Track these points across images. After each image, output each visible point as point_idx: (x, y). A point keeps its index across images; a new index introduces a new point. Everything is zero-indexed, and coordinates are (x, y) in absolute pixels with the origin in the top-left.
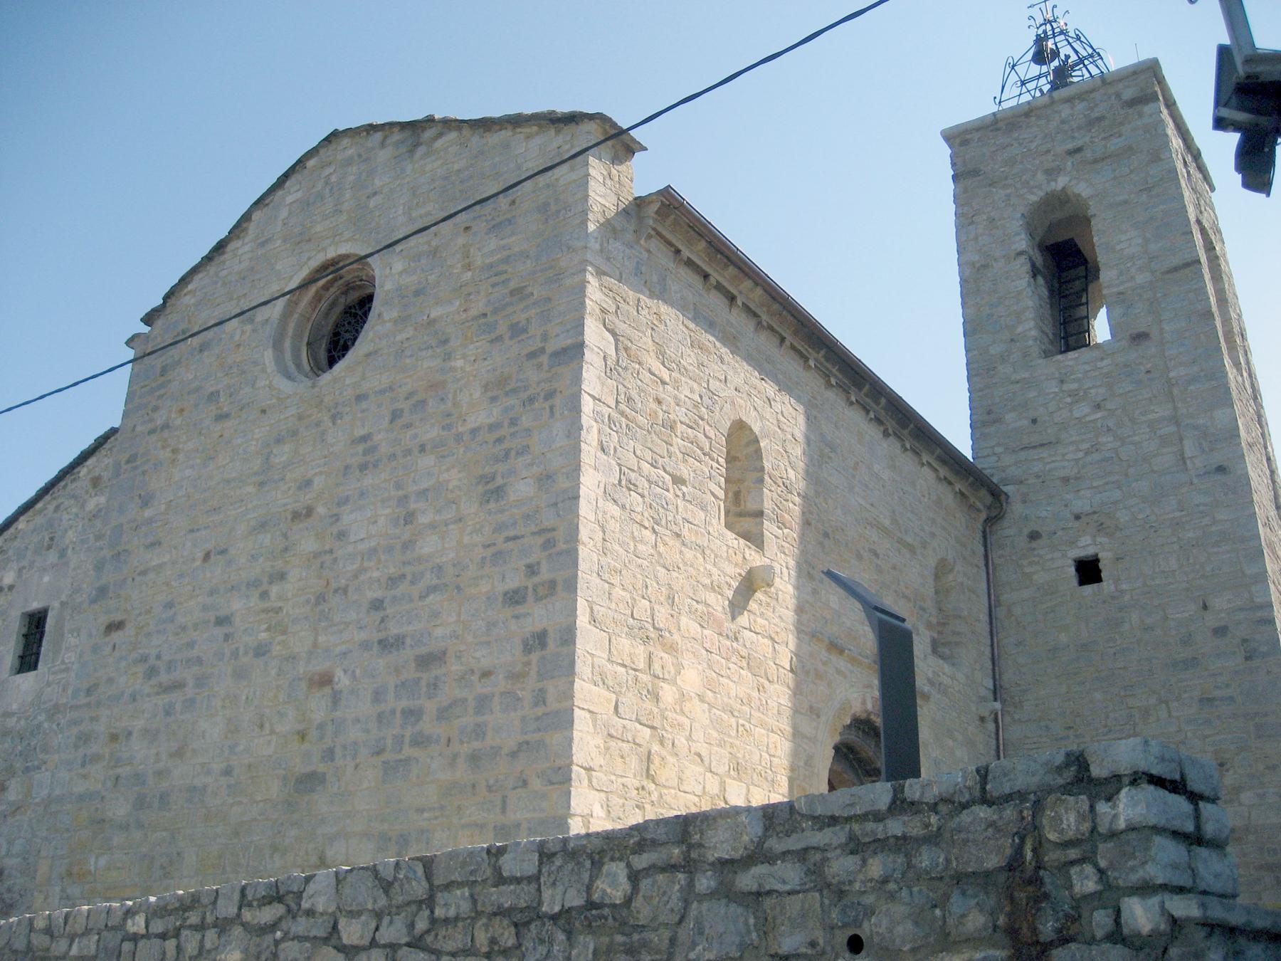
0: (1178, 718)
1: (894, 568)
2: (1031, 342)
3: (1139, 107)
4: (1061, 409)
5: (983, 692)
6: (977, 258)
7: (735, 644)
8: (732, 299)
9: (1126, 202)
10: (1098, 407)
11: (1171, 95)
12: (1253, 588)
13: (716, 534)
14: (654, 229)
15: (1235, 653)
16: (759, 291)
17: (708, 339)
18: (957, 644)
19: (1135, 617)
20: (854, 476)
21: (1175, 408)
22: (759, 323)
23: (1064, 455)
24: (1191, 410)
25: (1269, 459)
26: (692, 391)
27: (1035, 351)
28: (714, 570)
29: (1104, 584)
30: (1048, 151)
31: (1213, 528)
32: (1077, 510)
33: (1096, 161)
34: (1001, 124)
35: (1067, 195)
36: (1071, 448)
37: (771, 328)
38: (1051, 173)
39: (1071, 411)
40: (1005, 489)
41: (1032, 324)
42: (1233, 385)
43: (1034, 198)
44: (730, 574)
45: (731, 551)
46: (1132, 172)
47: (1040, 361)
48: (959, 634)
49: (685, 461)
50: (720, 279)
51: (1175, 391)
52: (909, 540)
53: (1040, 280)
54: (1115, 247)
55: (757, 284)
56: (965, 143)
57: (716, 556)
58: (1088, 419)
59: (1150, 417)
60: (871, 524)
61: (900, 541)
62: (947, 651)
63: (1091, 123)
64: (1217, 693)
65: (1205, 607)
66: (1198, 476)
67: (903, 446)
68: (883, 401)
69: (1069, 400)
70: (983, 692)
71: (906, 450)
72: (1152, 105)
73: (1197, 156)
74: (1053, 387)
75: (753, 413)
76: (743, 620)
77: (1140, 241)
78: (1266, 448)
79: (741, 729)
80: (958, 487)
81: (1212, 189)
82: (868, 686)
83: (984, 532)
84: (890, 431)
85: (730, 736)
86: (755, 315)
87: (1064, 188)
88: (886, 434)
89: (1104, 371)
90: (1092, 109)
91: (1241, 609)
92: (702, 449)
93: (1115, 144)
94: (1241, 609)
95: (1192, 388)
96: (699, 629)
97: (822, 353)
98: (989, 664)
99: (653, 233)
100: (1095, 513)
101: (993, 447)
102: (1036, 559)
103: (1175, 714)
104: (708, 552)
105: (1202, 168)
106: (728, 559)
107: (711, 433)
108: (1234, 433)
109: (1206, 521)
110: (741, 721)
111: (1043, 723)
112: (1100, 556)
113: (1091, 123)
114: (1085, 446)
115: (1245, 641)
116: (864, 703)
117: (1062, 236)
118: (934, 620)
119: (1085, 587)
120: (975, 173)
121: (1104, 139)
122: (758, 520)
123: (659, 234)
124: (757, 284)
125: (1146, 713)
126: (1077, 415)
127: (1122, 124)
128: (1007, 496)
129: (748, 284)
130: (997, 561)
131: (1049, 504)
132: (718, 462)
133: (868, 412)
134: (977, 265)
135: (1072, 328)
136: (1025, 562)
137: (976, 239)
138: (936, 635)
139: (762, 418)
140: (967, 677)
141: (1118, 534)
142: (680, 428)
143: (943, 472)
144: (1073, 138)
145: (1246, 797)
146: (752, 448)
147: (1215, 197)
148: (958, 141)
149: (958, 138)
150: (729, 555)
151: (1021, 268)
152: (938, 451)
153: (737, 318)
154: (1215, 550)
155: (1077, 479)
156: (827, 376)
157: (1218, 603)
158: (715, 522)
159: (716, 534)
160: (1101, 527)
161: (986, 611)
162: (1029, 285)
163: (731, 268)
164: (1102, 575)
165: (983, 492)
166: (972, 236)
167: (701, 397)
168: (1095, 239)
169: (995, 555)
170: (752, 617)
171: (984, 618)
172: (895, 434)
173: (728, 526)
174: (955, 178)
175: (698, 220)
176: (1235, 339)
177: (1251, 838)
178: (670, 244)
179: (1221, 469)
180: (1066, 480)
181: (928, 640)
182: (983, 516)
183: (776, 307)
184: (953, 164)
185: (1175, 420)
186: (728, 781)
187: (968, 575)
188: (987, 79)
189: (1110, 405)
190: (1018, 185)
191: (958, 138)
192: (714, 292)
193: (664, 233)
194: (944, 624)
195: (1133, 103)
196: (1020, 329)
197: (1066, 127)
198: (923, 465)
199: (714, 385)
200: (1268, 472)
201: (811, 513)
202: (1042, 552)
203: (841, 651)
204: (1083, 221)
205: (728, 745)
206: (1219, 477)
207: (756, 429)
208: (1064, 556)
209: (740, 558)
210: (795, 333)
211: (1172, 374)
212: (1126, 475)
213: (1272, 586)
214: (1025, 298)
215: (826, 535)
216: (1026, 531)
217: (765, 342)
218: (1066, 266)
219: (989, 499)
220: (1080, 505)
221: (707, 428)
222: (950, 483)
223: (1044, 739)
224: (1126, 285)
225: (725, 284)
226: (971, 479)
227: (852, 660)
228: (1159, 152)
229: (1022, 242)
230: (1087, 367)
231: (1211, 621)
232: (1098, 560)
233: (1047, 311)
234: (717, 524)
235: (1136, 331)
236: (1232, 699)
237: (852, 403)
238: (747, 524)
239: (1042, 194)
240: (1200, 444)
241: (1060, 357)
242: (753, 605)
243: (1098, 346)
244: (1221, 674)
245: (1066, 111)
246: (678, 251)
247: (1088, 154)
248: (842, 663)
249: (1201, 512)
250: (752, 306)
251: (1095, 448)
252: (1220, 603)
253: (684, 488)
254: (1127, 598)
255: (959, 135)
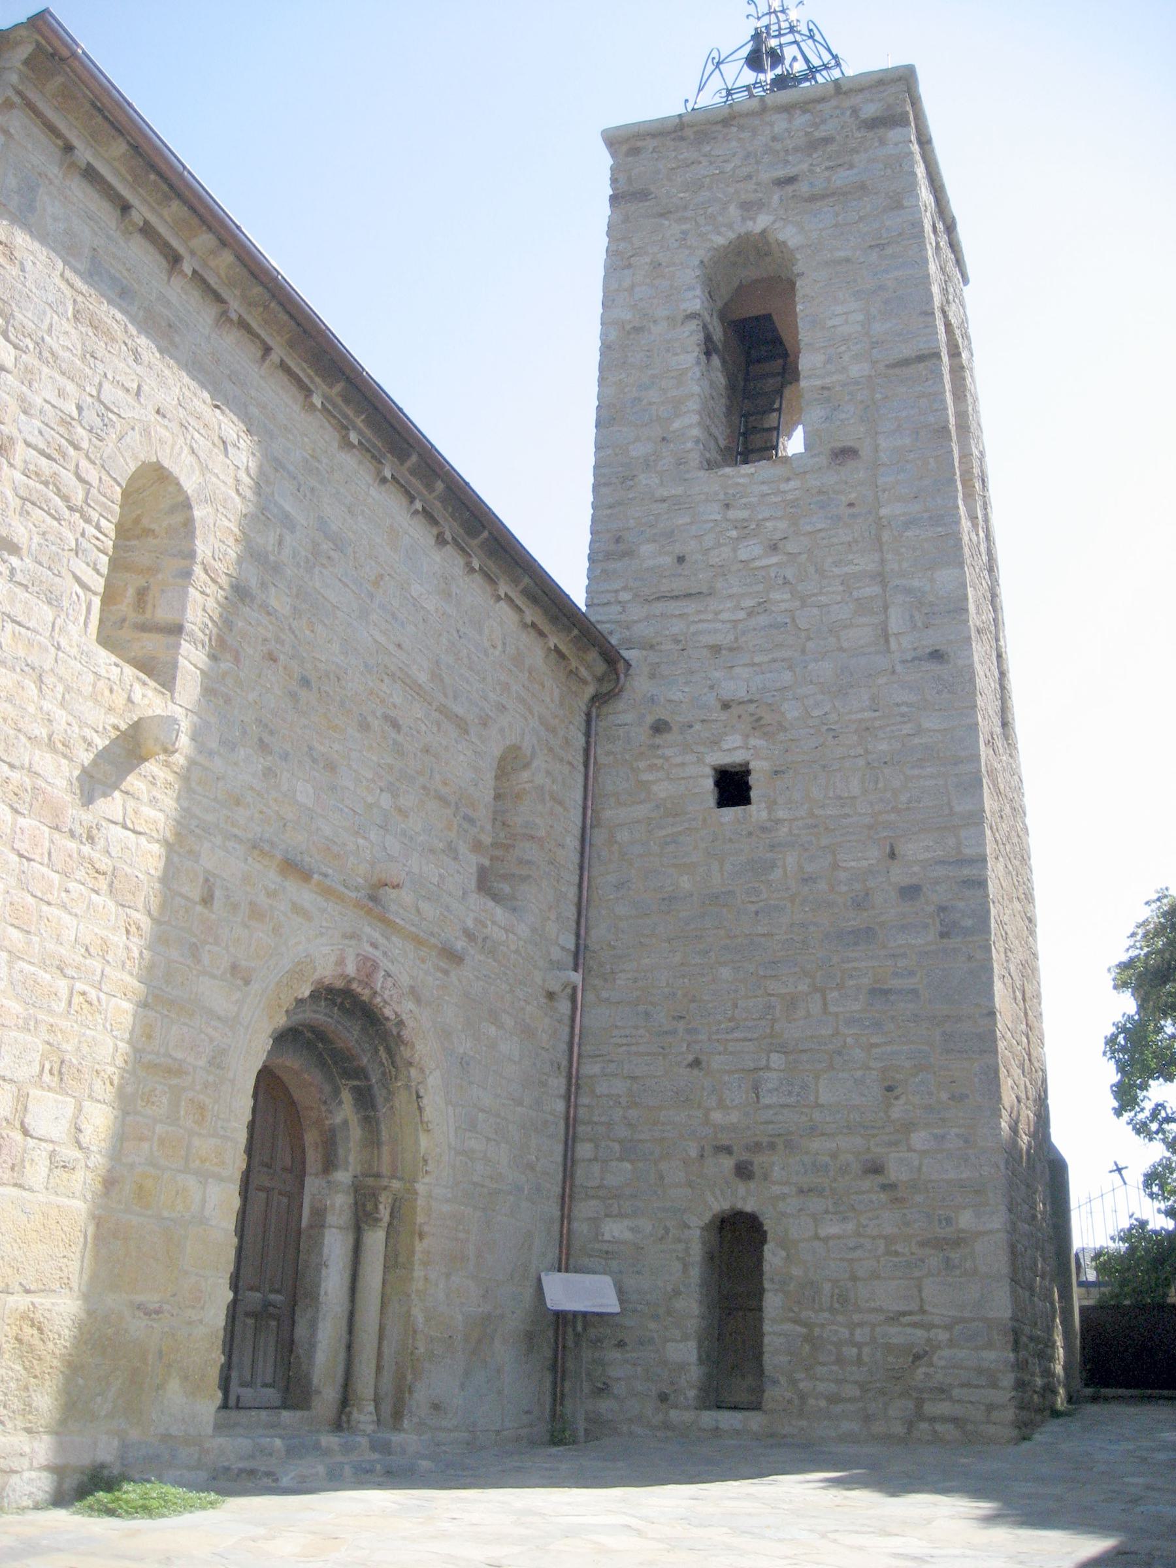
0: (836, 1015)
1: (427, 750)
2: (689, 445)
3: (881, 131)
4: (720, 545)
5: (556, 954)
6: (629, 317)
7: (86, 849)
8: (174, 260)
9: (848, 260)
10: (774, 548)
11: (927, 127)
12: (963, 833)
13: (74, 651)
14: (19, 93)
15: (926, 926)
16: (227, 257)
17: (111, 315)
18: (525, 879)
19: (791, 860)
20: (371, 596)
21: (883, 561)
22: (224, 313)
23: (716, 614)
24: (905, 565)
25: (999, 656)
26: (61, 393)
27: (695, 458)
28: (61, 716)
29: (752, 808)
30: (749, 177)
31: (916, 741)
32: (727, 695)
33: (813, 199)
34: (689, 133)
35: (767, 243)
36: (729, 604)
37: (243, 325)
38: (749, 208)
39: (735, 550)
40: (625, 653)
41: (695, 418)
42: (966, 539)
43: (720, 241)
44: (98, 727)
45: (101, 684)
46: (861, 219)
47: (702, 473)
48: (529, 862)
49: (25, 513)
50: (153, 220)
51: (886, 536)
52: (459, 710)
53: (716, 361)
54: (827, 333)
55: (223, 243)
56: (635, 151)
57: (68, 689)
58: (757, 564)
59: (846, 569)
60: (392, 676)
61: (442, 710)
62: (507, 889)
63: (814, 145)
64: (895, 983)
65: (892, 855)
66: (904, 662)
67: (468, 564)
68: (440, 486)
69: (734, 533)
70: (556, 954)
71: (472, 570)
72: (899, 130)
73: (950, 228)
74: (713, 512)
75: (187, 458)
76: (112, 805)
77: (861, 317)
78: (997, 640)
79: (77, 999)
80: (553, 641)
81: (966, 281)
82: (353, 936)
83: (588, 715)
84: (448, 536)
85: (50, 1011)
86: (218, 298)
87: (764, 231)
88: (441, 540)
89: (789, 497)
90: (816, 126)
91: (942, 862)
92: (66, 499)
93: (841, 178)
94: (942, 862)
95: (908, 534)
96: (8, 815)
97: (339, 387)
98: (571, 912)
99: (16, 99)
100: (751, 701)
101: (616, 591)
102: (659, 762)
103: (832, 1009)
104: (49, 680)
105: (954, 246)
106: (94, 697)
107: (92, 474)
108: (959, 608)
109: (907, 729)
110: (79, 986)
111: (641, 1008)
112: (751, 767)
113: (814, 145)
114: (749, 603)
115: (942, 909)
116: (341, 962)
117: (754, 309)
118: (487, 840)
119: (725, 810)
120: (642, 195)
121: (827, 168)
122: (171, 639)
123: (30, 106)
124: (223, 243)
125: (792, 1003)
126: (744, 557)
127: (855, 151)
128: (628, 665)
129: (204, 240)
130: (603, 760)
131: (687, 683)
132: (98, 527)
133: (412, 499)
134: (628, 327)
135: (757, 440)
136: (642, 765)
137: (632, 287)
138: (487, 863)
139: (204, 469)
140: (534, 930)
141: (781, 736)
142: (20, 452)
143: (532, 614)
144: (787, 162)
145: (919, 1139)
146: (178, 518)
147: (967, 291)
148: (625, 148)
149: (626, 144)
150: (104, 691)
151: (690, 337)
152: (526, 580)
153: (178, 295)
154: (916, 772)
155: (731, 650)
156: (343, 428)
157: (911, 849)
158: (74, 630)
159: (74, 651)
160: (757, 724)
161: (577, 831)
162: (698, 363)
163: (175, 205)
164: (753, 794)
165: (593, 655)
166: (627, 283)
167: (79, 408)
168: (799, 308)
169: (599, 751)
170: (131, 803)
171: (572, 843)
172: (457, 544)
173: (105, 640)
174: (614, 199)
175: (106, 90)
176: (974, 482)
177: (919, 1198)
178: (51, 129)
179: (937, 656)
180: (716, 649)
181: (474, 870)
182: (590, 690)
183: (257, 290)
184: (614, 181)
185: (880, 577)
186: (34, 1092)
187: (552, 777)
188: (680, 70)
189: (791, 547)
190: (701, 220)
191: (626, 144)
192: (138, 239)
193: (41, 105)
194: (507, 847)
195: (874, 124)
196: (676, 425)
197: (778, 146)
198: (499, 598)
199: (110, 393)
200: (996, 673)
201: (280, 641)
202: (668, 752)
203: (305, 875)
204: (783, 286)
205: (44, 1028)
206: (934, 667)
207: (190, 484)
208: (700, 761)
209: (119, 700)
210: (291, 344)
211: (883, 512)
212: (803, 651)
213: (988, 832)
214: (690, 385)
215: (305, 682)
216: (650, 720)
217: (233, 349)
218: (754, 356)
219: (601, 667)
220: (733, 688)
221: (84, 464)
222: (541, 634)
223: (641, 1031)
224: (835, 378)
225: (162, 229)
226: (576, 632)
227: (327, 892)
228: (900, 199)
229: (695, 301)
230: (765, 489)
231: (899, 875)
232: (748, 772)
233: (720, 406)
234: (80, 627)
235: (839, 445)
236: (914, 992)
237: (384, 480)
238: (151, 643)
239: (732, 235)
240: (912, 616)
241: (728, 470)
242: (133, 782)
243: (786, 459)
244: (904, 955)
245: (780, 124)
246: (69, 148)
247: (803, 188)
248: (307, 896)
249: (903, 715)
250: (212, 281)
251: (763, 606)
252: (914, 849)
253: (14, 561)
254: (784, 830)
255: (628, 140)
